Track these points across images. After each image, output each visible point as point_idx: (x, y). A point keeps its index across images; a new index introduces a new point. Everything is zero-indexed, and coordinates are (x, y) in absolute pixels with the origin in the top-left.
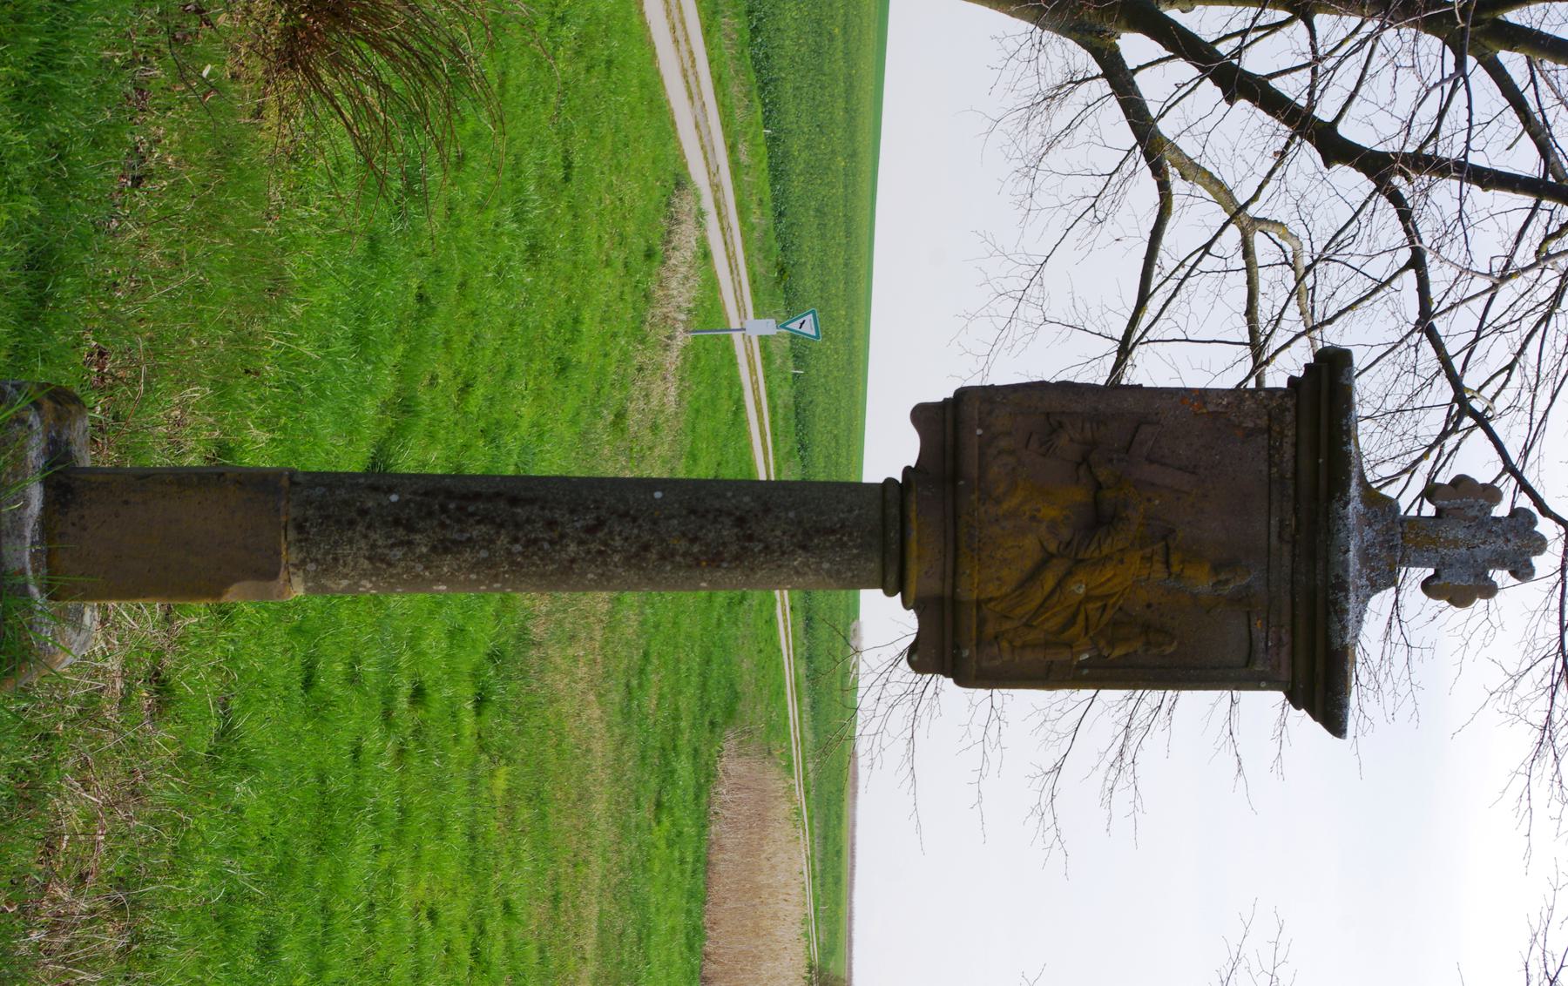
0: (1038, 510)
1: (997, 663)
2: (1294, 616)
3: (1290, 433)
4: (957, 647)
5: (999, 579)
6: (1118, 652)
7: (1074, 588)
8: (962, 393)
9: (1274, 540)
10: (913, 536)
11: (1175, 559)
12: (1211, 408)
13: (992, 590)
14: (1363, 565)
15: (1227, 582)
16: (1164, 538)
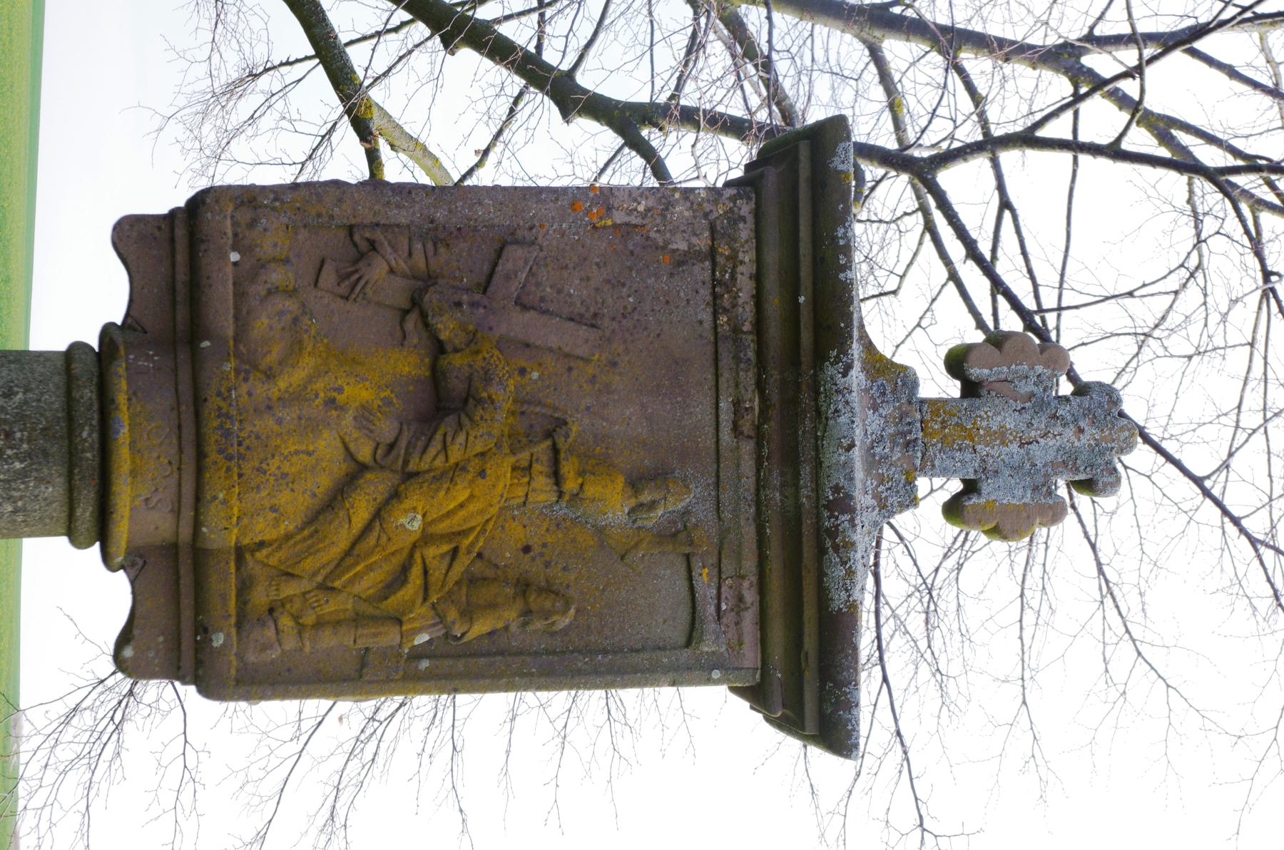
0: (340, 390)
1: (274, 654)
2: (762, 560)
3: (748, 257)
4: (203, 630)
5: (273, 509)
6: (480, 627)
7: (402, 520)
8: (198, 203)
9: (726, 436)
10: (123, 435)
11: (569, 468)
12: (619, 217)
13: (263, 529)
14: (868, 472)
15: (652, 505)
16: (549, 435)
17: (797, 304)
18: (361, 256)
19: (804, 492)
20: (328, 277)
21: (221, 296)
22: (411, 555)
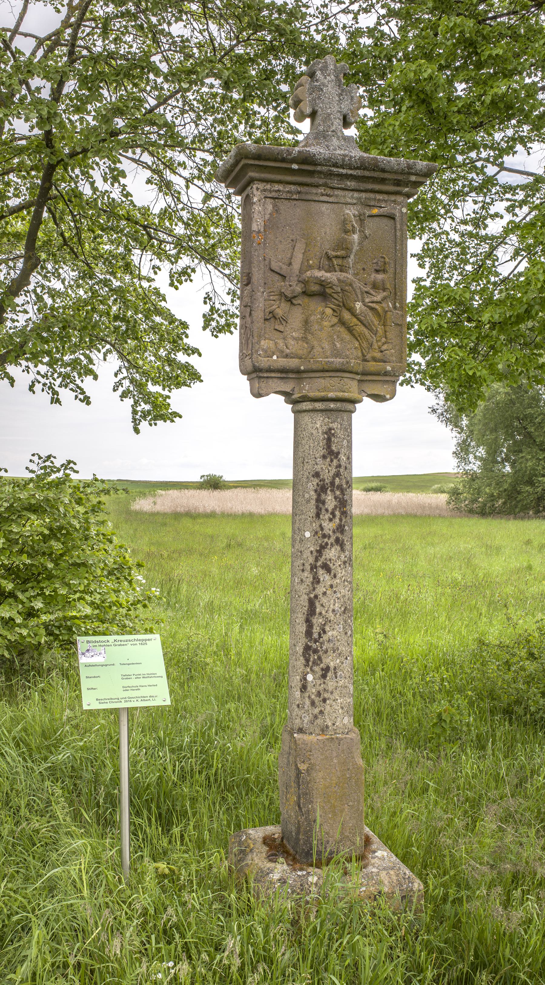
17: (299, 170)
18: (274, 317)
19: (165, 236)
20: (281, 328)
21: (283, 362)
22: (368, 307)
